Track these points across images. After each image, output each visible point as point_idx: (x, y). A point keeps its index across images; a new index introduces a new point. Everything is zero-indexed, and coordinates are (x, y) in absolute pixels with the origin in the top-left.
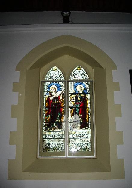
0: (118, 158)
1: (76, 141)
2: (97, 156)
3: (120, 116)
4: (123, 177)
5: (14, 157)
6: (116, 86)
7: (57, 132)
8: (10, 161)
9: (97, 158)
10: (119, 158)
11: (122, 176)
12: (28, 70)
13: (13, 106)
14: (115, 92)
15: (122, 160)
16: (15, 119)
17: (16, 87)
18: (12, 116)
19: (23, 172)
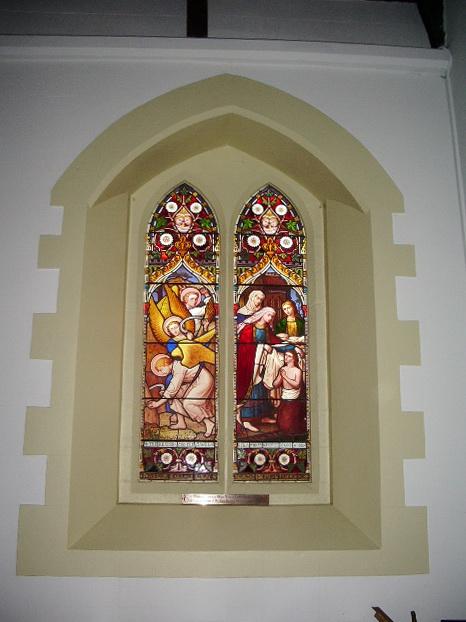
0: (408, 503)
1: (272, 421)
2: (332, 496)
3: (416, 360)
4: (422, 568)
5: (37, 497)
6: (405, 259)
7: (158, 494)
8: (27, 513)
9: (332, 503)
10: (412, 4)
11: (416, 561)
12: (91, 206)
13: (39, 320)
14: (398, 279)
15: (421, 512)
16: (46, 365)
17: (49, 253)
18: (36, 352)
19: (75, 547)
